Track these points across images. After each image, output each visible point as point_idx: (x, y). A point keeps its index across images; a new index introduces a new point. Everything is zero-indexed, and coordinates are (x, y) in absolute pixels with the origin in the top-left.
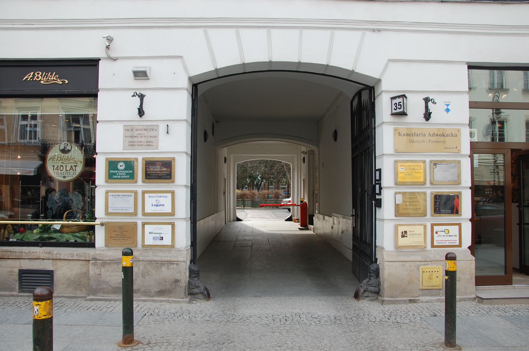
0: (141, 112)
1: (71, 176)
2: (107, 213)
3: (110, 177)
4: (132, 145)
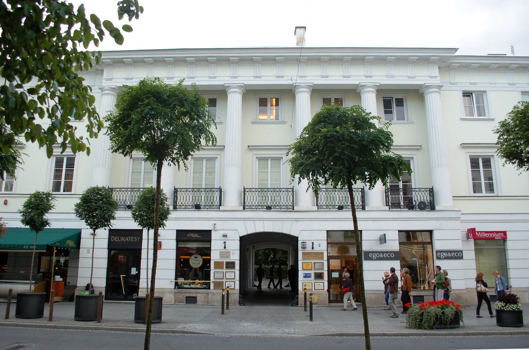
0: (225, 247)
1: (198, 266)
2: (214, 278)
3: (215, 267)
4: (222, 257)
